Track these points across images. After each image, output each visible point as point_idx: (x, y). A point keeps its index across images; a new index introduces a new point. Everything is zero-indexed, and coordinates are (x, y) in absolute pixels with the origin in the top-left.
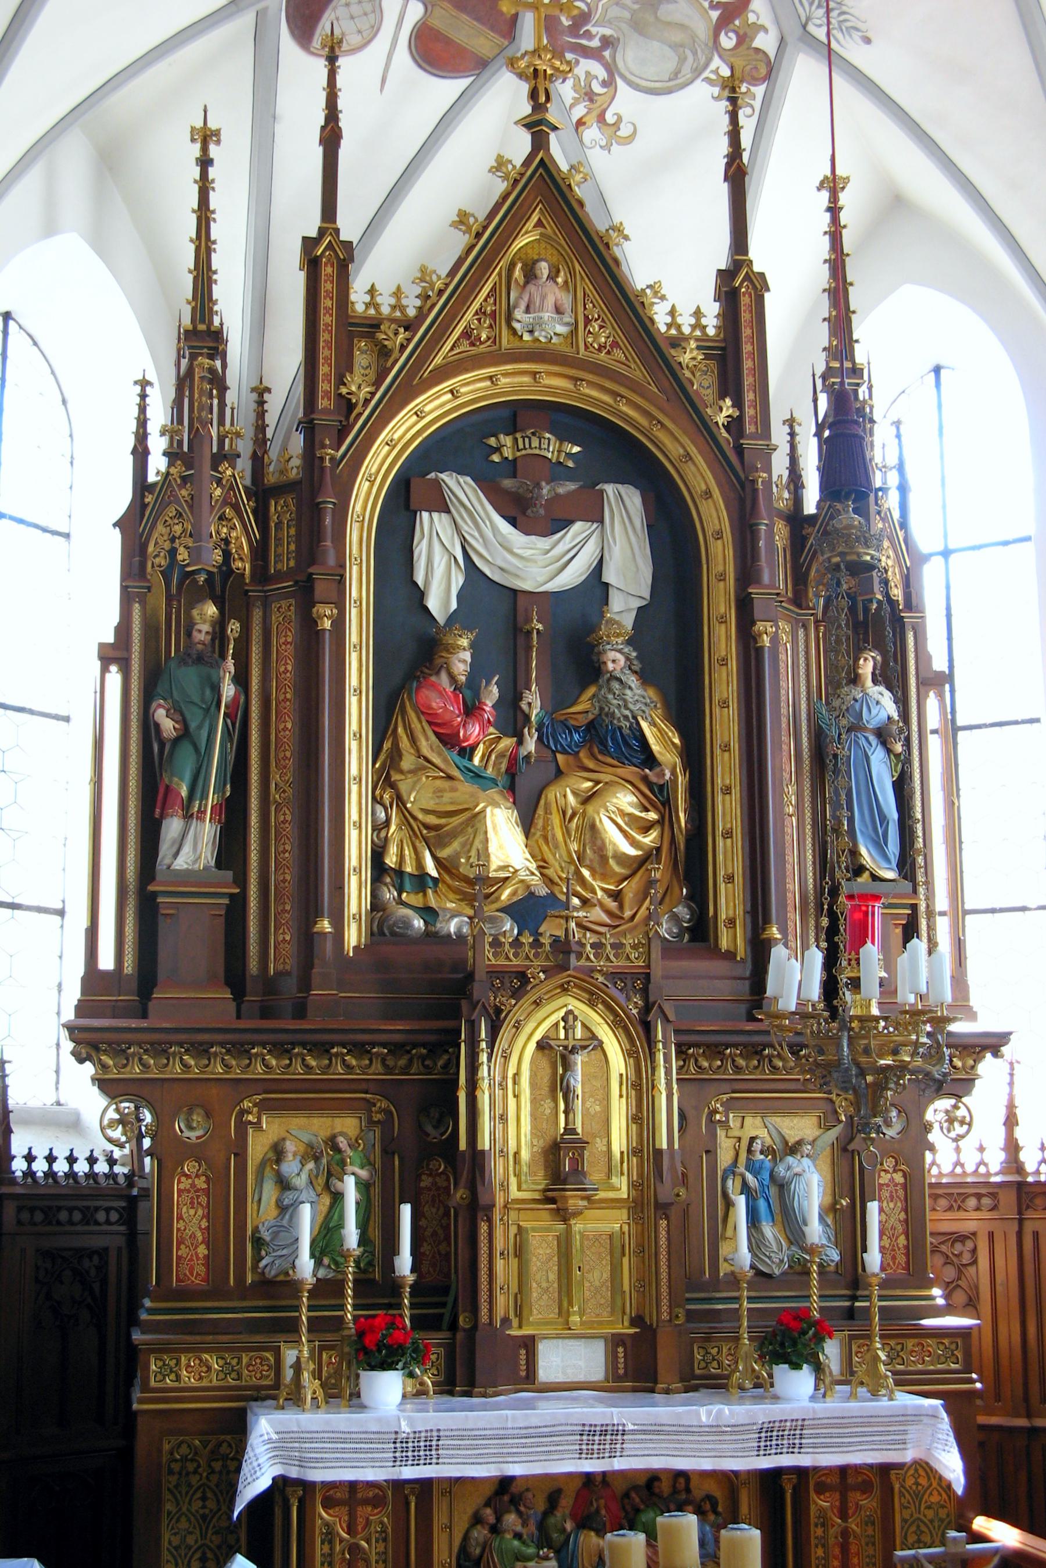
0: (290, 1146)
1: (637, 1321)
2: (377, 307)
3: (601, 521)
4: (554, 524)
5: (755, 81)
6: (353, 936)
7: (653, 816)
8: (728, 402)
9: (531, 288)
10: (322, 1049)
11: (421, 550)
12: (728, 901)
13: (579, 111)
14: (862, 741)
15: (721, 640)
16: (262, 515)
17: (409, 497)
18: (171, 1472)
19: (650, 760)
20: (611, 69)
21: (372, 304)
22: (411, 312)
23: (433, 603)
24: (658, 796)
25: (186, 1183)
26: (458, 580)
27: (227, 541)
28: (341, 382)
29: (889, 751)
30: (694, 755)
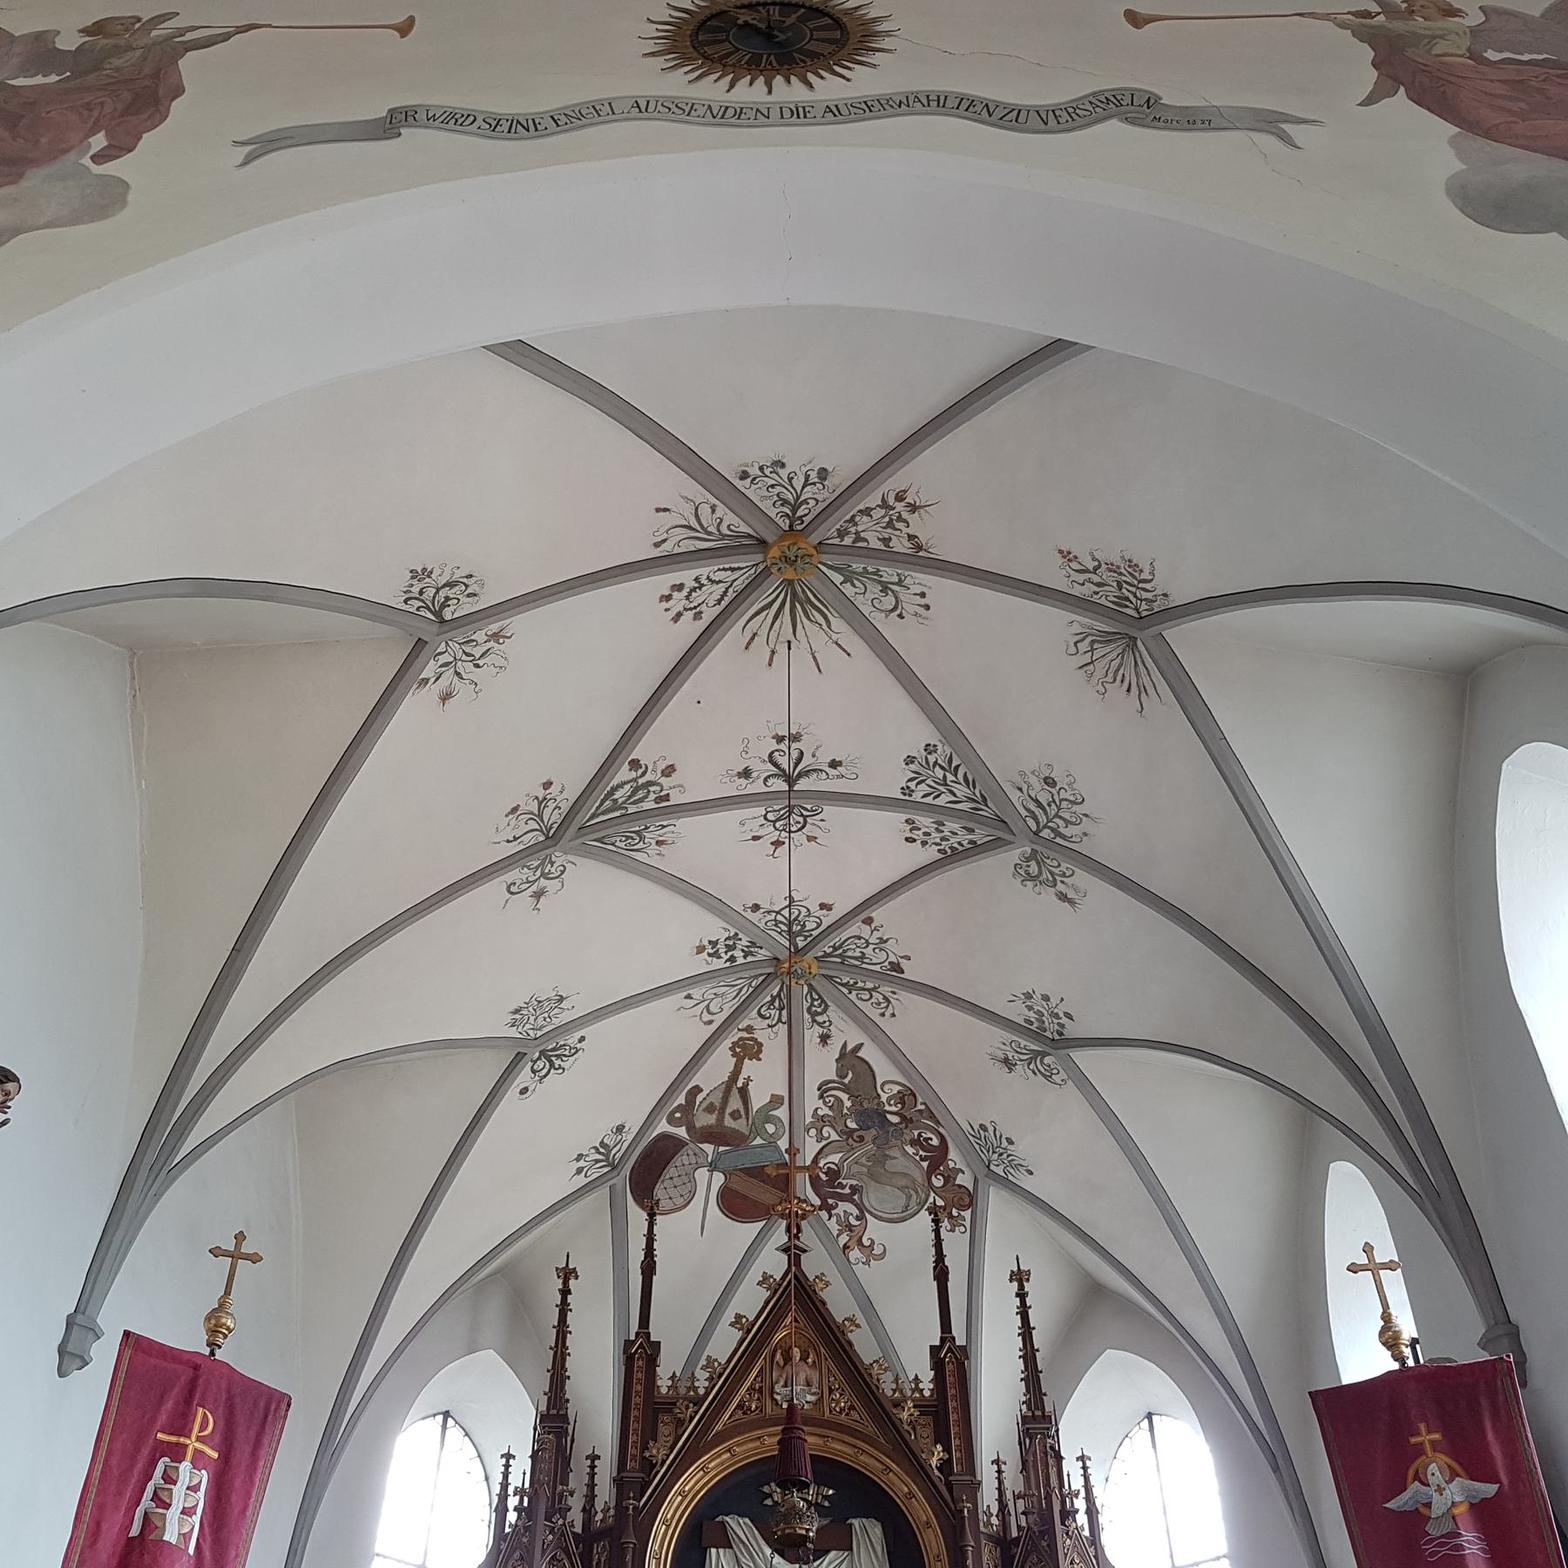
5: (962, 1208)
8: (939, 1447)
9: (788, 1367)
13: (844, 1239)
20: (861, 1208)
21: (673, 1387)
22: (701, 1391)
28: (645, 1448)
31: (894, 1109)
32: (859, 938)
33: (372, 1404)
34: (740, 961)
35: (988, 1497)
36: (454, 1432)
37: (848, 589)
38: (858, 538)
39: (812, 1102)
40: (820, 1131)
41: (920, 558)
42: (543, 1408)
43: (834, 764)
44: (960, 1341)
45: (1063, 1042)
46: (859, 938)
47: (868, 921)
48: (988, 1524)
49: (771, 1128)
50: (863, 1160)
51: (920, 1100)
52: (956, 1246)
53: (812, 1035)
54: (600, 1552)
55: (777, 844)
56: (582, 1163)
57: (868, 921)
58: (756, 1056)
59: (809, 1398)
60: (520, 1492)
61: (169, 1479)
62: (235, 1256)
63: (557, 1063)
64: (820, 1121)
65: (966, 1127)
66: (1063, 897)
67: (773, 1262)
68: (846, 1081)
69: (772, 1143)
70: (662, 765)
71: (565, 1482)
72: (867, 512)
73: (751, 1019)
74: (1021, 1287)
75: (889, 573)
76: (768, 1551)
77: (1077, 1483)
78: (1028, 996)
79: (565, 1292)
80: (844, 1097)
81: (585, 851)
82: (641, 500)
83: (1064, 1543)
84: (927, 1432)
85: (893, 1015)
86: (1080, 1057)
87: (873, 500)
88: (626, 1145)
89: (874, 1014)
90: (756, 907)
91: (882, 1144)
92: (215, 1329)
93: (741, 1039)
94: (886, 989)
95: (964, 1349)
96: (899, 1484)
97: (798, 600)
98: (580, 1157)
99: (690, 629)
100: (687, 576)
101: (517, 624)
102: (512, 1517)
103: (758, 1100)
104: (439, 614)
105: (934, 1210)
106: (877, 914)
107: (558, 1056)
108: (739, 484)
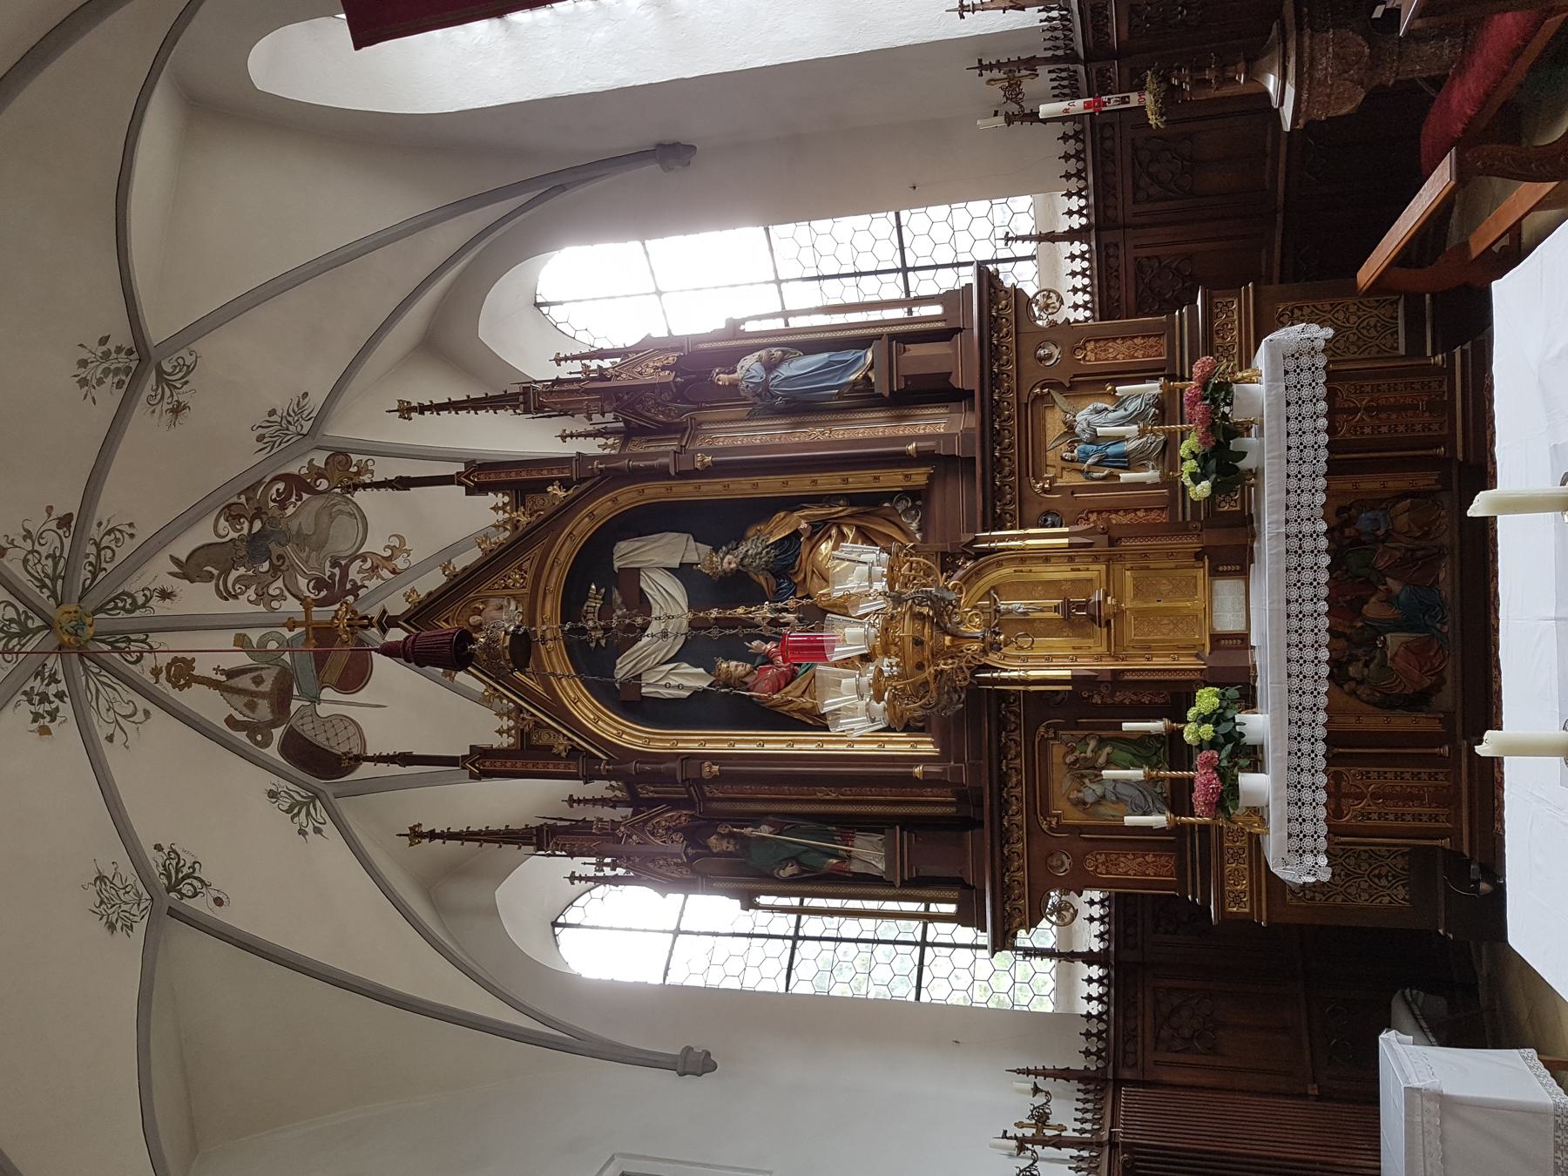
0: (1074, 795)
1: (1198, 557)
2: (509, 729)
3: (639, 569)
4: (642, 603)
5: (349, 463)
6: (927, 748)
7: (834, 532)
10: (1003, 779)
11: (666, 693)
12: (892, 479)
13: (386, 574)
14: (775, 382)
15: (713, 489)
16: (652, 803)
17: (634, 704)
18: (1313, 898)
19: (796, 534)
23: (704, 684)
24: (820, 529)
25: (1102, 869)
26: (685, 668)
27: (669, 828)
28: (558, 756)
29: (782, 360)
30: (793, 503)
31: (246, 525)
32: (25, 561)
33: (538, 1007)
34: (63, 686)
35: (591, 447)
36: (571, 916)
40: (274, 598)
42: (531, 849)
44: (461, 468)
46: (25, 561)
48: (612, 447)
50: (304, 555)
51: (235, 500)
52: (386, 469)
53: (160, 608)
54: (646, 792)
56: (310, 829)
58: (190, 664)
59: (513, 607)
60: (600, 866)
63: (186, 870)
64: (262, 596)
65: (262, 455)
68: (216, 572)
69: (288, 645)
73: (143, 671)
74: (414, 409)
76: (645, 640)
77: (577, 366)
80: (234, 575)
83: (625, 380)
85: (131, 525)
88: (291, 786)
91: (286, 538)
93: (169, 680)
94: (95, 533)
95: (468, 464)
96: (582, 526)
98: (302, 832)
102: (620, 871)
107: (177, 872)
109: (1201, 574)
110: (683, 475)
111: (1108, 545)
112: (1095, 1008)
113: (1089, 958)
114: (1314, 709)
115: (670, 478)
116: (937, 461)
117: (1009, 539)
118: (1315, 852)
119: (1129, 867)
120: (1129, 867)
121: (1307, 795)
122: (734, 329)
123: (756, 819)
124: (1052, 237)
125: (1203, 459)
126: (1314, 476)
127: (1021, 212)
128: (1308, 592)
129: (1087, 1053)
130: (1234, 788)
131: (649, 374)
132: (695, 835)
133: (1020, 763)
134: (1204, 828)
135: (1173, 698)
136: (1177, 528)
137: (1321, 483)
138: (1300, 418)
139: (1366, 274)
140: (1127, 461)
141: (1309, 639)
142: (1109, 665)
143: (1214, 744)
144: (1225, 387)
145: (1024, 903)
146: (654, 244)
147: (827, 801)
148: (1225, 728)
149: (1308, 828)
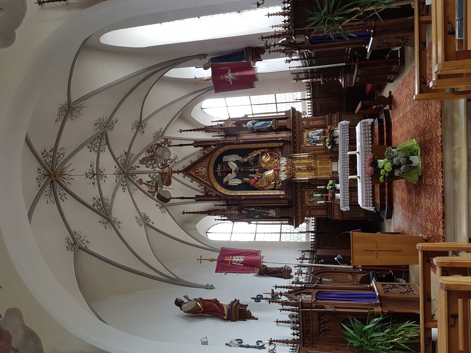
5: (168, 141)
6: (283, 193)
10: (297, 198)
11: (233, 184)
12: (276, 145)
13: (174, 163)
15: (243, 146)
16: (231, 205)
19: (258, 155)
24: (263, 154)
26: (237, 180)
30: (257, 149)
36: (210, 231)
37: (59, 164)
38: (50, 162)
39: (150, 169)
41: (54, 150)
43: (91, 166)
44: (193, 142)
45: (140, 122)
47: (118, 159)
49: (155, 177)
52: (174, 142)
55: (105, 177)
57: (118, 159)
58: (142, 180)
61: (235, 262)
62: (201, 260)
64: (153, 167)
66: (116, 122)
67: (180, 176)
69: (157, 177)
70: (93, 200)
71: (219, 210)
72: (45, 160)
73: (135, 181)
75: (57, 155)
78: (132, 128)
79: (187, 213)
81: (111, 213)
82: (46, 206)
83: (226, 126)
84: (209, 148)
86: (143, 119)
87: (43, 159)
89: (134, 157)
90: (116, 181)
92: (212, 260)
96: (218, 153)
97: (62, 174)
99: (68, 196)
100: (59, 196)
101: (73, 229)
102: (225, 218)
103: (151, 180)
104: (73, 245)
105: (170, 146)
106: (117, 157)
108: (41, 186)
109: (330, 161)
110: (237, 144)
111: (314, 156)
112: (313, 240)
113: (312, 232)
114: (347, 183)
115: (235, 144)
116: (284, 141)
117: (298, 155)
118: (347, 206)
119: (318, 213)
120: (318, 213)
121: (346, 197)
122: (246, 116)
123: (251, 207)
124: (304, 100)
125: (330, 142)
126: (347, 145)
127: (298, 95)
128: (346, 164)
129: (311, 248)
130: (335, 196)
131: (230, 125)
132: (240, 210)
133: (300, 195)
134: (331, 203)
135: (325, 182)
136: (326, 153)
137: (348, 146)
138: (345, 136)
139: (357, 111)
140: (318, 142)
141: (346, 171)
142: (315, 177)
143: (331, 189)
144: (333, 131)
145: (300, 220)
146: (227, 99)
147: (264, 203)
148: (333, 186)
149: (346, 202)
